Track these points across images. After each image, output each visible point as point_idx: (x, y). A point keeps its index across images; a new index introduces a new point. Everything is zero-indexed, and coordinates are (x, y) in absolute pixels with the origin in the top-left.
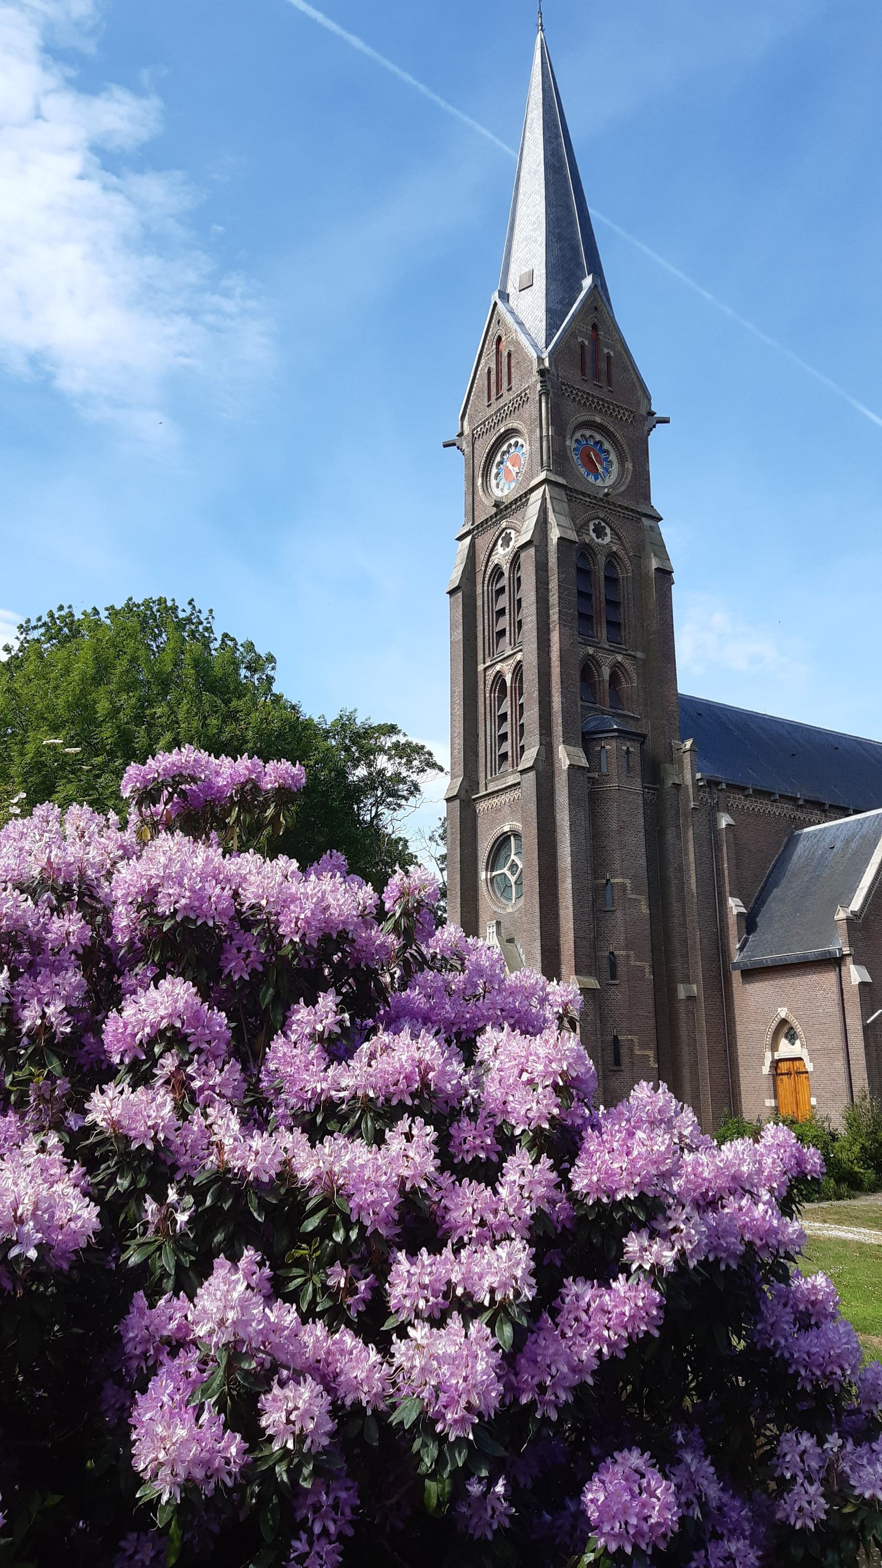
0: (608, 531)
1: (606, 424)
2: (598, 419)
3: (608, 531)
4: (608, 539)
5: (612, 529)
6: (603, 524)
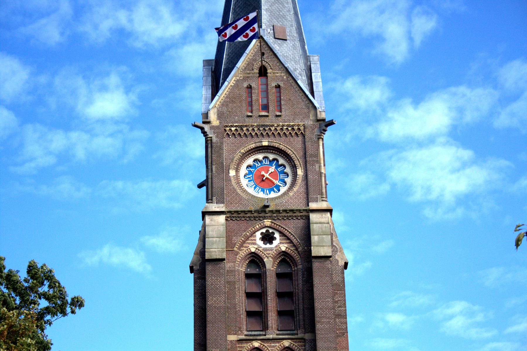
0: (277, 235)
3: (277, 235)
4: (275, 243)
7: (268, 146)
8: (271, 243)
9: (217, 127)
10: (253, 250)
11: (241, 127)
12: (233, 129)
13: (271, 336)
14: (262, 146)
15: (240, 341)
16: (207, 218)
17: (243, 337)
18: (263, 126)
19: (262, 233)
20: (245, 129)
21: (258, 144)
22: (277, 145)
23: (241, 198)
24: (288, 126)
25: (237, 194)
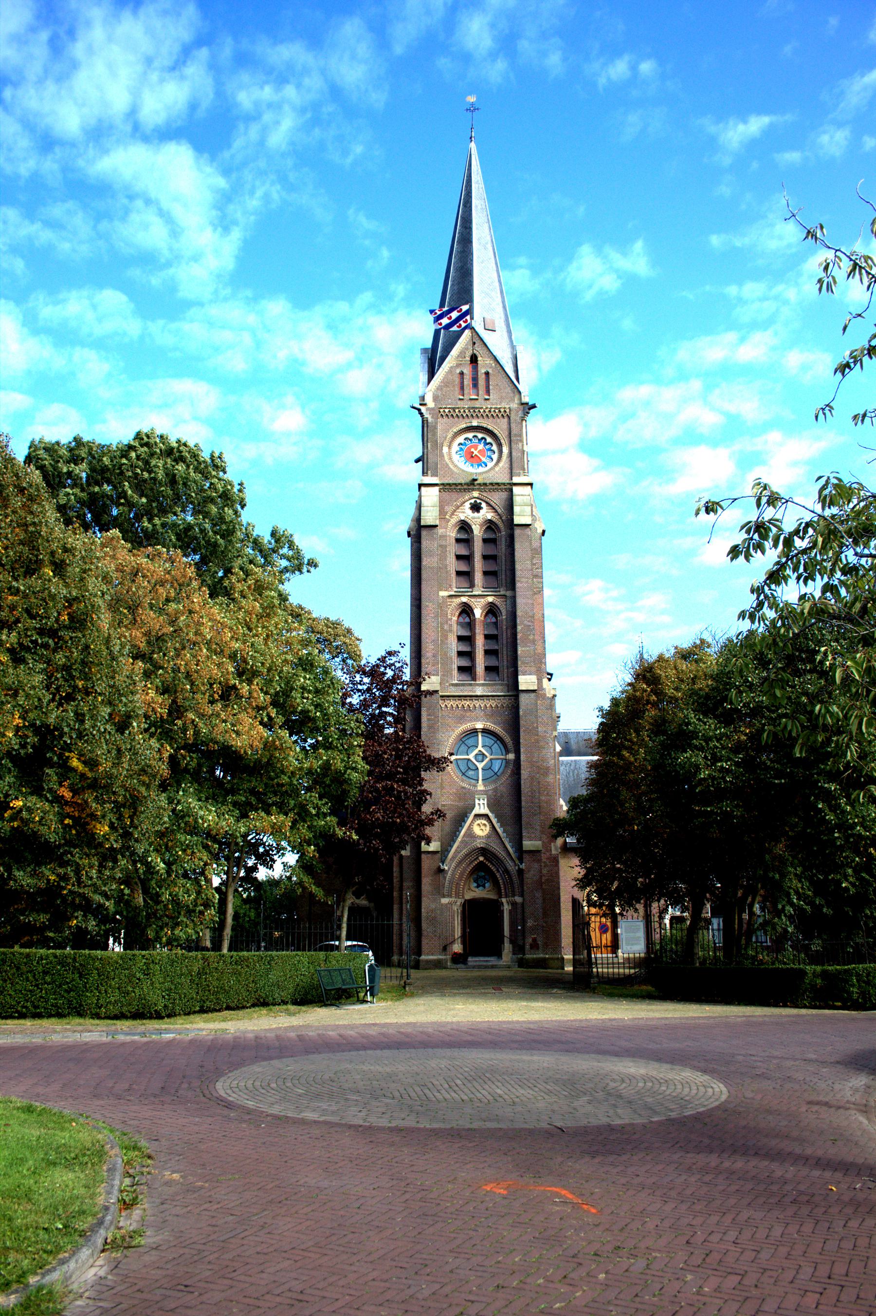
0: (484, 505)
3: (484, 505)
8: (478, 511)
9: (432, 409)
11: (454, 409)
12: (447, 410)
15: (451, 596)
16: (423, 489)
17: (453, 593)
18: (473, 408)
21: (469, 425)
22: (485, 426)
23: (453, 472)
24: (496, 408)
25: (449, 468)
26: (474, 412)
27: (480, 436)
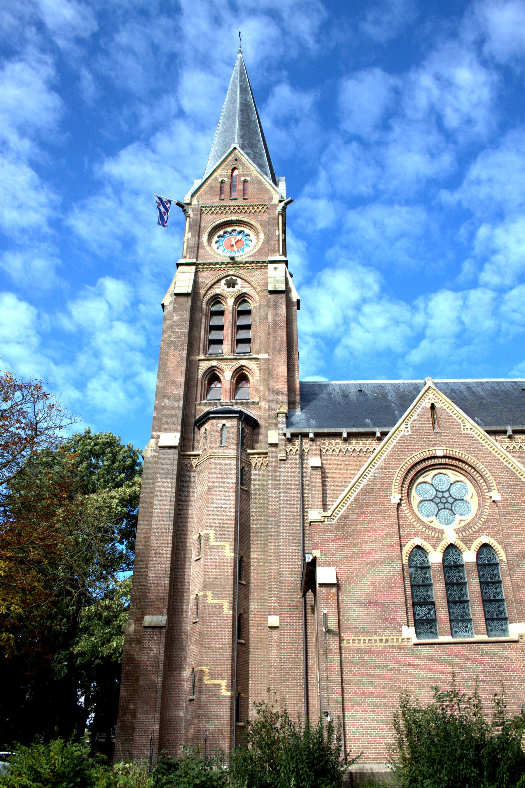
0: (239, 281)
1: (241, 219)
2: (234, 218)
3: (239, 281)
5: (242, 279)
6: (234, 278)
7: (236, 220)
8: (233, 287)
10: (218, 292)
13: (228, 357)
14: (232, 220)
19: (225, 284)
20: (232, 208)
26: (239, 209)
27: (221, 233)
